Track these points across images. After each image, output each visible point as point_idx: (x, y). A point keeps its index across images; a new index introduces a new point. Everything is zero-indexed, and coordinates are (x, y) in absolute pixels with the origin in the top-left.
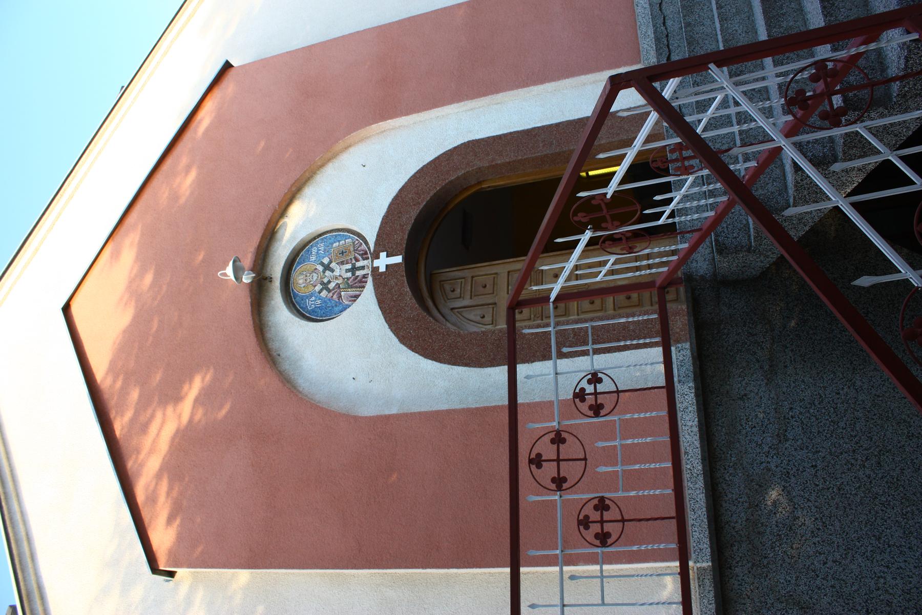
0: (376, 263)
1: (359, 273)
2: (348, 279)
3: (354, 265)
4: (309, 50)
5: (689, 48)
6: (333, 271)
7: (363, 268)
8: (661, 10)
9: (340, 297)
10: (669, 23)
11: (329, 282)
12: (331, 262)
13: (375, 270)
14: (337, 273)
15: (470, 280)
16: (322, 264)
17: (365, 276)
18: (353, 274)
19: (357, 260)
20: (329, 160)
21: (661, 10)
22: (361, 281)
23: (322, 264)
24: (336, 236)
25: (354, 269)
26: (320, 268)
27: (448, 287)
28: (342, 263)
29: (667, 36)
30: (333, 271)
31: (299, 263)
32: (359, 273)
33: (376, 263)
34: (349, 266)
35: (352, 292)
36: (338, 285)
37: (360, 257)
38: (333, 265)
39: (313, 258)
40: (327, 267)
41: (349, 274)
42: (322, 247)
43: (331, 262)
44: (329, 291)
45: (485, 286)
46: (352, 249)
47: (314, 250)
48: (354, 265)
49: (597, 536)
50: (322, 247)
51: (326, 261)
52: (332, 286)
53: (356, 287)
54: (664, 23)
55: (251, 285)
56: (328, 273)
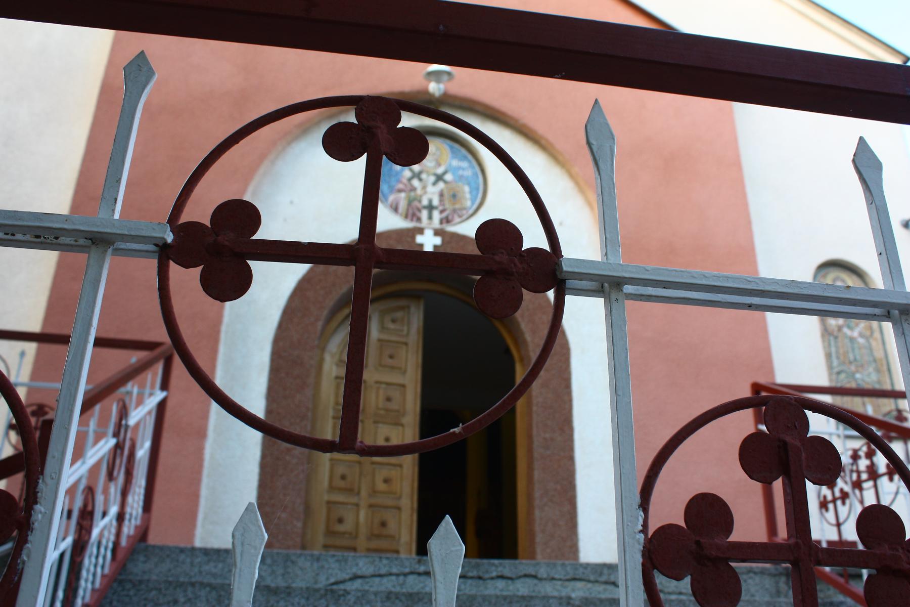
0: (429, 233)
1: (424, 214)
2: (420, 201)
3: (436, 208)
4: (736, 164)
5: (403, 594)
6: (434, 184)
7: (430, 217)
8: (526, 576)
9: (400, 191)
10: (500, 584)
11: (420, 180)
12: (445, 182)
13: (421, 231)
14: (430, 189)
15: (404, 340)
16: (445, 173)
17: (419, 220)
18: (425, 207)
19: (442, 212)
20: (577, 183)
21: (526, 576)
22: (414, 215)
23: (445, 173)
24: (477, 189)
25: (430, 208)
26: (440, 171)
27: (399, 314)
28: (441, 195)
29: (480, 578)
30: (434, 184)
31: (451, 148)
32: (424, 214)
33: (429, 233)
34: (436, 202)
35: (403, 205)
36: (414, 189)
37: (444, 215)
38: (441, 185)
39: (455, 163)
40: (439, 178)
41: (425, 202)
42: (468, 173)
43: (445, 182)
44: (410, 180)
45: (391, 357)
46: (457, 206)
47: (465, 164)
48: (436, 208)
49: (708, 511)
50: (468, 173)
51: (448, 177)
52: (416, 183)
53: (408, 210)
54: (502, 577)
55: (426, 92)
56: (432, 179)
